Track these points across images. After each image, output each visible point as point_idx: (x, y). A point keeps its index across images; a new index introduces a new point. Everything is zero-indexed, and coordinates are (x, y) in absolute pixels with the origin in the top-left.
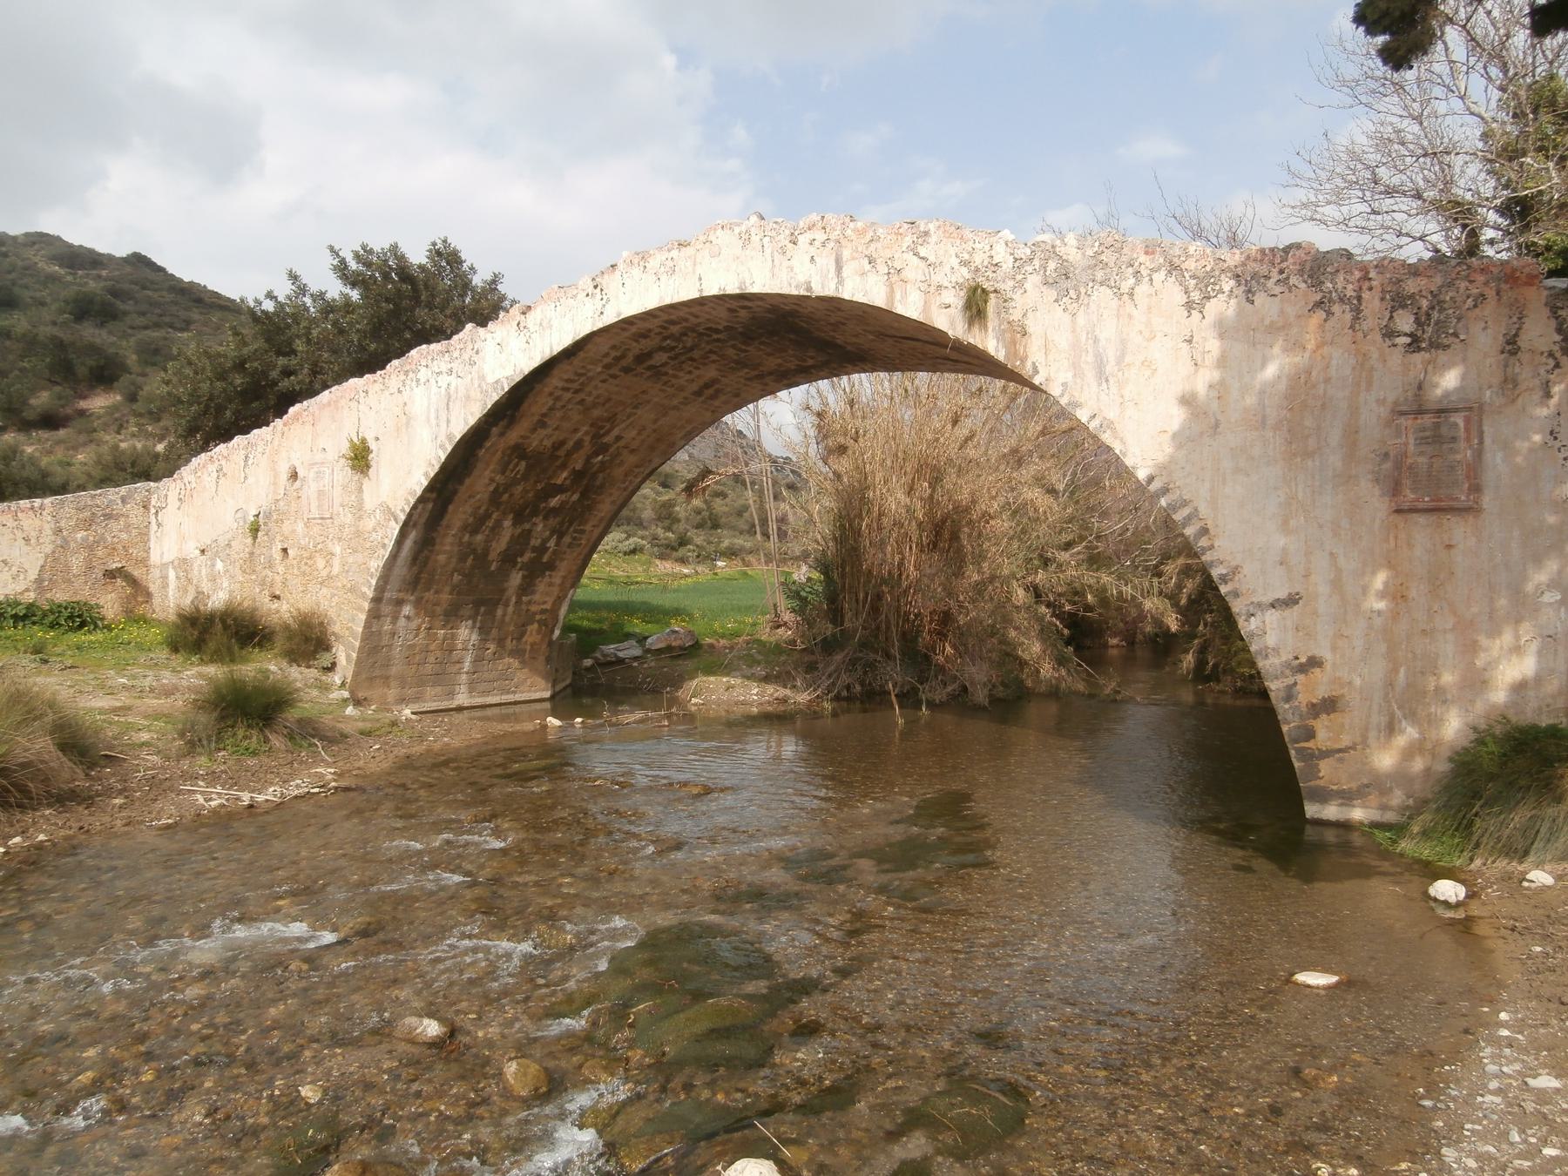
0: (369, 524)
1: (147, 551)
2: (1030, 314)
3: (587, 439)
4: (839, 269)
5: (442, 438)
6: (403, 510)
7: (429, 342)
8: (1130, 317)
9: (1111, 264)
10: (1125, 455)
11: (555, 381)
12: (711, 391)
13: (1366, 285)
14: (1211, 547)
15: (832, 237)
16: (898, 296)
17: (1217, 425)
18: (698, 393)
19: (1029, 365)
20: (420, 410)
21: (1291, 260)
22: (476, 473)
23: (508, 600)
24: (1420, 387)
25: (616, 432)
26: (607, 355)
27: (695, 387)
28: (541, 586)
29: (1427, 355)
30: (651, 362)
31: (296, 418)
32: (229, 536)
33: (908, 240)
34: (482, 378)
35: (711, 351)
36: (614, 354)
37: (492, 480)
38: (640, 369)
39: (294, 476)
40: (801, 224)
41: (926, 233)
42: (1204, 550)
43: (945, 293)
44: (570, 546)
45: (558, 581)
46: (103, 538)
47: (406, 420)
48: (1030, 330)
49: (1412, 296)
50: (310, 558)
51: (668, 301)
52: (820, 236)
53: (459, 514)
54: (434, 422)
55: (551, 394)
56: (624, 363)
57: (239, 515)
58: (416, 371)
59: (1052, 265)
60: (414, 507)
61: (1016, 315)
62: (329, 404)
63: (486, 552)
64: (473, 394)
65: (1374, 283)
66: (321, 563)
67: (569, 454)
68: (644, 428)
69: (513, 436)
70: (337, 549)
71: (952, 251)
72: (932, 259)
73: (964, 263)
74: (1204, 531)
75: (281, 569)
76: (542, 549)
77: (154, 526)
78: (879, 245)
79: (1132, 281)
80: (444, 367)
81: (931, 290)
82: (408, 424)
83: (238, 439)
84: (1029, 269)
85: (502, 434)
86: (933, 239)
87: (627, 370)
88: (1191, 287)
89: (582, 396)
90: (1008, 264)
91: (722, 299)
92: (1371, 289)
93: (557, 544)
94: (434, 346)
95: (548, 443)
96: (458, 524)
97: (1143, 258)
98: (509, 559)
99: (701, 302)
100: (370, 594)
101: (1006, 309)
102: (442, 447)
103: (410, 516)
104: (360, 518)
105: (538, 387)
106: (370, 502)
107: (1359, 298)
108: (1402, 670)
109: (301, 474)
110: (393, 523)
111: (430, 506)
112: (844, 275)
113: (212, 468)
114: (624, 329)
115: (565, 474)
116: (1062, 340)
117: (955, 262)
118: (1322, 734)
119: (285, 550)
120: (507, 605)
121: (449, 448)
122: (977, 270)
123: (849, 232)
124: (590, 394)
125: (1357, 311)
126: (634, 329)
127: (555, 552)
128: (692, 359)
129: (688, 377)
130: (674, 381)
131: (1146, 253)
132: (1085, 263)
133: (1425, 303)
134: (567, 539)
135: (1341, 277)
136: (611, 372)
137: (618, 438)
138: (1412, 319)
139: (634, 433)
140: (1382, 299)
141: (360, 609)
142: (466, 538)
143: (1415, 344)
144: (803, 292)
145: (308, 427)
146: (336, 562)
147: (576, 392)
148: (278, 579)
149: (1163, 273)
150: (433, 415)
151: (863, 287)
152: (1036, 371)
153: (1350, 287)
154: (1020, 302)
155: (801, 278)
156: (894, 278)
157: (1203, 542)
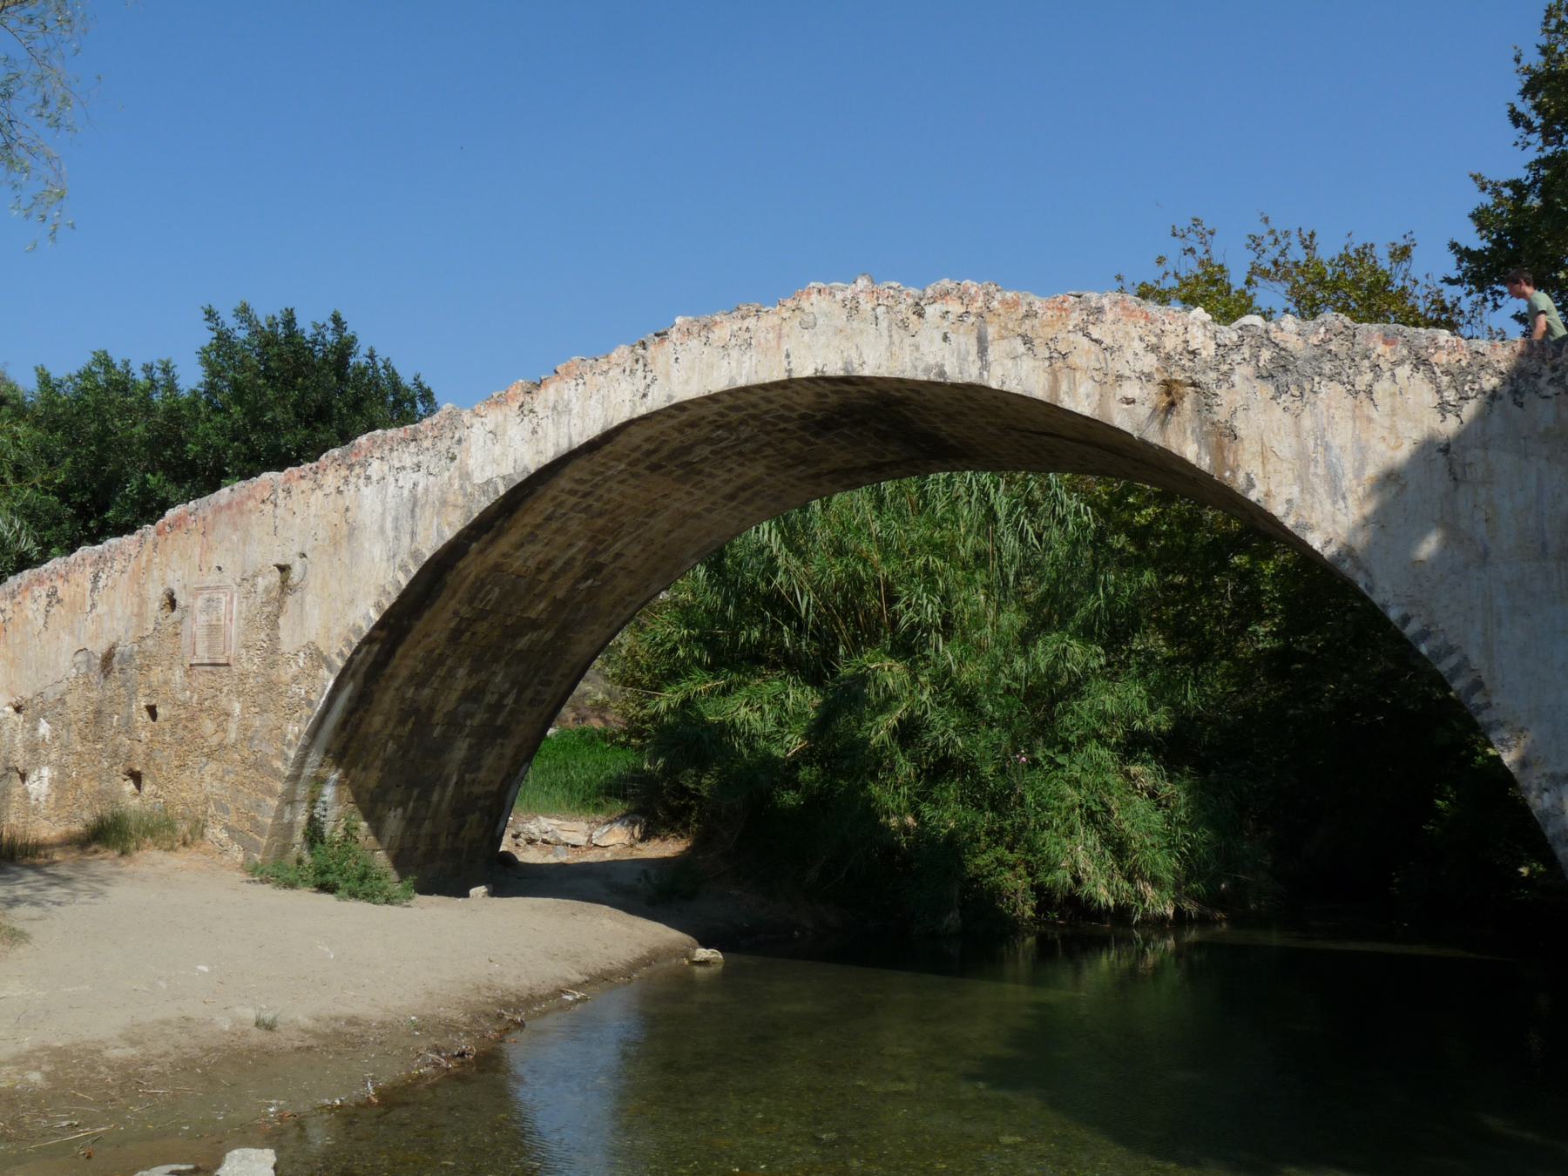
0: (286, 673)
2: (1240, 414)
3: (581, 557)
4: (982, 350)
5: (404, 555)
6: (341, 654)
8: (1370, 420)
10: (1371, 589)
11: (564, 482)
12: (748, 494)
14: (1488, 705)
15: (973, 309)
16: (1064, 387)
17: (1485, 555)
18: (731, 497)
22: (439, 604)
23: (448, 779)
27: (728, 489)
30: (690, 458)
32: (63, 687)
33: (1076, 318)
34: (466, 476)
35: (769, 444)
36: (646, 447)
37: (456, 613)
38: (671, 467)
40: (929, 292)
41: (1100, 310)
42: (1479, 709)
43: (1126, 385)
45: (509, 751)
47: (346, 533)
48: (1241, 433)
50: (193, 719)
51: (742, 382)
52: (956, 308)
53: (407, 661)
55: (554, 498)
57: (80, 657)
58: (365, 465)
59: (1266, 354)
60: (357, 651)
61: (1221, 414)
62: (229, 506)
63: (431, 710)
64: (451, 498)
66: (209, 726)
69: (494, 555)
70: (237, 708)
71: (1135, 333)
72: (1108, 341)
73: (1154, 349)
74: (1478, 685)
78: (1036, 322)
79: (1369, 376)
80: (408, 461)
81: (1109, 380)
83: (85, 551)
84: (1238, 358)
85: (482, 551)
86: (1109, 317)
89: (590, 500)
90: (1208, 352)
93: (516, 701)
94: (391, 432)
95: (532, 563)
97: (1381, 348)
98: (454, 722)
99: (788, 384)
101: (1209, 407)
102: (404, 568)
103: (350, 661)
104: (273, 665)
105: (541, 489)
106: (289, 639)
109: (181, 600)
110: (324, 672)
111: (376, 648)
113: (41, 592)
114: (671, 417)
116: (1284, 446)
117: (1138, 346)
119: (152, 711)
120: (445, 786)
121: (414, 571)
122: (1168, 357)
123: (995, 304)
126: (684, 417)
128: (740, 454)
129: (726, 476)
130: (707, 481)
131: (1386, 343)
132: (1308, 353)
134: (529, 694)
136: (635, 470)
137: (618, 556)
142: (410, 693)
144: (933, 377)
145: (196, 538)
146: (233, 727)
147: (586, 495)
148: (140, 749)
150: (389, 525)
154: (1226, 399)
155: (931, 360)
157: (1477, 699)
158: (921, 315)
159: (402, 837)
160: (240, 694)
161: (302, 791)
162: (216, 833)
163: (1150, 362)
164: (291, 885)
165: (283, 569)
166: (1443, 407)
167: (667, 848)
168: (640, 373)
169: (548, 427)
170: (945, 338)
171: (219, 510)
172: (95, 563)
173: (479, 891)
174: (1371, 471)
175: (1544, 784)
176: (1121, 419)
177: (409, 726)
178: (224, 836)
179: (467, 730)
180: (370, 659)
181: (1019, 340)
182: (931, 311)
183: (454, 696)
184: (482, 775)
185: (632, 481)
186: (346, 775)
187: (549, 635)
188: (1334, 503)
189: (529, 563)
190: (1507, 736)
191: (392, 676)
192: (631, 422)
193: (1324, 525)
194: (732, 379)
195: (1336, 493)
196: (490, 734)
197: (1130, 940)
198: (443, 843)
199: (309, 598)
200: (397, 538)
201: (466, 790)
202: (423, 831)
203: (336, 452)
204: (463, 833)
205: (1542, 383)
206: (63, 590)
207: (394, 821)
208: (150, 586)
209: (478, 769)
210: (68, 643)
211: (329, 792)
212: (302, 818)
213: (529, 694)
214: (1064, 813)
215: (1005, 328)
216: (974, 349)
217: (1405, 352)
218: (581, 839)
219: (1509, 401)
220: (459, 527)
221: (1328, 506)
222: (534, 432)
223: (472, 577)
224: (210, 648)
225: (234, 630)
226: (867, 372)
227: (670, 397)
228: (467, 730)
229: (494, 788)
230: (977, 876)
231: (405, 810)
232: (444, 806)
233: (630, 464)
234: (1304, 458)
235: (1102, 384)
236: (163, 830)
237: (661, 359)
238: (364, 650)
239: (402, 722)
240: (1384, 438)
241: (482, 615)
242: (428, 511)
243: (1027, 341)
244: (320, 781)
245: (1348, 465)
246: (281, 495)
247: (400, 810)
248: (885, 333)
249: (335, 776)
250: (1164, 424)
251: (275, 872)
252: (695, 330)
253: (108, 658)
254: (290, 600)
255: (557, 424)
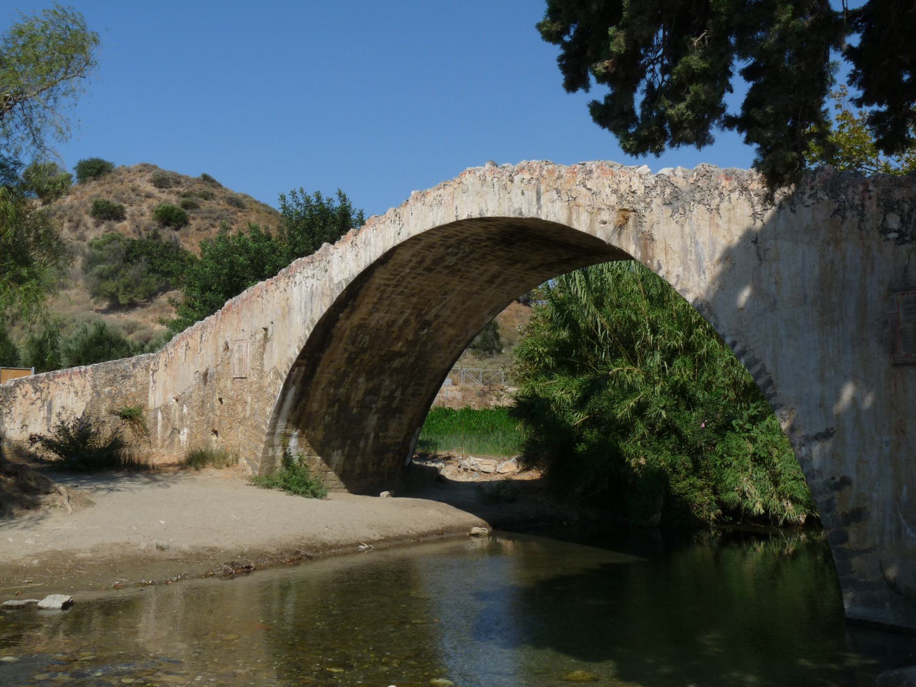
1: (147, 401)
2: (655, 226)
3: (413, 318)
4: (539, 199)
6: (285, 372)
7: (302, 257)
8: (718, 226)
9: (705, 189)
11: (379, 278)
12: (500, 279)
13: (867, 196)
14: (775, 394)
15: (535, 177)
16: (574, 217)
17: (775, 302)
18: (490, 282)
19: (655, 262)
20: (293, 303)
21: (818, 180)
24: (906, 270)
25: (434, 311)
26: (410, 261)
27: (485, 277)
28: (393, 425)
29: (910, 246)
30: (447, 263)
31: (228, 310)
32: (191, 389)
33: (580, 177)
34: (331, 280)
36: (415, 260)
37: (346, 350)
39: (227, 348)
41: (591, 172)
43: (603, 213)
44: (413, 395)
46: (120, 392)
48: (656, 237)
49: (898, 202)
51: (438, 224)
52: (527, 176)
54: (303, 311)
55: (377, 289)
56: (425, 265)
58: (294, 276)
59: (668, 191)
60: (292, 370)
61: (646, 227)
63: (348, 399)
64: (325, 291)
65: (872, 194)
66: (240, 408)
67: (401, 329)
68: (455, 308)
69: (356, 319)
70: (249, 400)
71: (607, 183)
72: (594, 189)
73: (615, 192)
74: (770, 382)
75: (218, 413)
76: (391, 398)
77: (151, 384)
78: (562, 181)
80: (310, 273)
82: (289, 311)
84: (654, 194)
85: (347, 318)
86: (595, 175)
87: (429, 270)
88: (755, 202)
90: (641, 192)
91: (470, 220)
92: (870, 198)
93: (402, 394)
96: (324, 382)
97: (724, 183)
98: (365, 406)
99: (458, 223)
100: (266, 429)
102: (308, 328)
103: (289, 376)
104: (261, 378)
105: (366, 285)
107: (863, 205)
108: (905, 488)
109: (230, 348)
110: (279, 381)
111: (303, 368)
112: (542, 203)
115: (400, 344)
117: (608, 190)
118: (852, 538)
119: (220, 400)
120: (367, 438)
121: (312, 329)
124: (406, 287)
125: (862, 215)
127: (401, 400)
129: (477, 271)
130: (468, 275)
131: (727, 179)
132: (688, 189)
133: (906, 207)
134: (410, 391)
135: (851, 190)
136: (418, 271)
137: (437, 316)
138: (898, 218)
139: (449, 312)
140: (878, 205)
141: (261, 440)
142: (332, 391)
143: (901, 238)
144: (517, 215)
146: (248, 408)
147: (396, 286)
149: (737, 193)
150: (303, 306)
151: (553, 211)
152: (660, 268)
153: (857, 197)
154: (649, 218)
155: (516, 206)
156: (572, 204)
157: (769, 391)
158: (512, 182)
159: (344, 465)
160: (251, 392)
161: (277, 440)
162: (243, 461)
163: (613, 199)
164: (268, 487)
165: (266, 329)
166: (754, 215)
167: (533, 475)
168: (397, 222)
169: (362, 254)
170: (523, 193)
171: (243, 301)
172: (201, 329)
173: (384, 494)
174: (718, 256)
175: (803, 442)
176: (600, 234)
177: (336, 408)
178: (245, 462)
179: (374, 411)
180: (302, 374)
181: (555, 192)
182: (517, 179)
183: (361, 392)
184: (391, 433)
185: (419, 277)
186: (303, 433)
187: (412, 360)
188: (699, 276)
189: (381, 322)
190: (784, 413)
191: (318, 383)
192: (394, 250)
193: (694, 289)
194: (434, 223)
195: (700, 270)
196: (388, 413)
197: (776, 535)
198: (371, 468)
199: (274, 344)
200: (306, 313)
201: (381, 441)
202: (356, 462)
203: (284, 270)
204: (383, 464)
205: (806, 197)
206: (192, 343)
207: (337, 457)
208: (220, 340)
209: (387, 430)
210: (193, 369)
211: (293, 442)
212: (279, 454)
213: (410, 391)
214: (740, 457)
215: (548, 185)
216: (535, 198)
217: (736, 184)
218: (491, 469)
219: (788, 209)
220: (328, 306)
221: (696, 279)
222: (357, 256)
223: (348, 332)
224: (239, 370)
225: (248, 360)
226: (489, 215)
227: (409, 234)
228: (374, 411)
229: (400, 440)
230: (679, 494)
231: (343, 452)
232: (368, 449)
233: (412, 268)
234: (685, 250)
235: (591, 213)
236: (222, 460)
237: (406, 214)
238: (296, 369)
239: (331, 405)
240: (724, 236)
241: (363, 350)
242: (317, 298)
243: (558, 192)
244: (287, 436)
245: (706, 253)
246: (265, 293)
247: (340, 451)
248: (497, 193)
249: (296, 433)
250: (620, 234)
251: (265, 481)
252: (419, 197)
253: (206, 374)
254: (268, 345)
255: (365, 251)
